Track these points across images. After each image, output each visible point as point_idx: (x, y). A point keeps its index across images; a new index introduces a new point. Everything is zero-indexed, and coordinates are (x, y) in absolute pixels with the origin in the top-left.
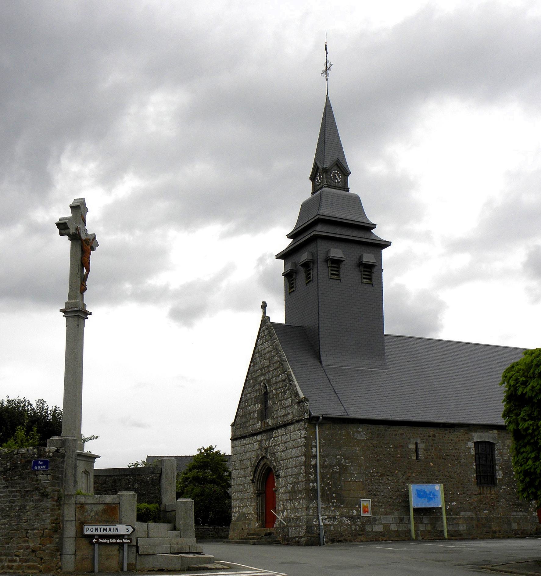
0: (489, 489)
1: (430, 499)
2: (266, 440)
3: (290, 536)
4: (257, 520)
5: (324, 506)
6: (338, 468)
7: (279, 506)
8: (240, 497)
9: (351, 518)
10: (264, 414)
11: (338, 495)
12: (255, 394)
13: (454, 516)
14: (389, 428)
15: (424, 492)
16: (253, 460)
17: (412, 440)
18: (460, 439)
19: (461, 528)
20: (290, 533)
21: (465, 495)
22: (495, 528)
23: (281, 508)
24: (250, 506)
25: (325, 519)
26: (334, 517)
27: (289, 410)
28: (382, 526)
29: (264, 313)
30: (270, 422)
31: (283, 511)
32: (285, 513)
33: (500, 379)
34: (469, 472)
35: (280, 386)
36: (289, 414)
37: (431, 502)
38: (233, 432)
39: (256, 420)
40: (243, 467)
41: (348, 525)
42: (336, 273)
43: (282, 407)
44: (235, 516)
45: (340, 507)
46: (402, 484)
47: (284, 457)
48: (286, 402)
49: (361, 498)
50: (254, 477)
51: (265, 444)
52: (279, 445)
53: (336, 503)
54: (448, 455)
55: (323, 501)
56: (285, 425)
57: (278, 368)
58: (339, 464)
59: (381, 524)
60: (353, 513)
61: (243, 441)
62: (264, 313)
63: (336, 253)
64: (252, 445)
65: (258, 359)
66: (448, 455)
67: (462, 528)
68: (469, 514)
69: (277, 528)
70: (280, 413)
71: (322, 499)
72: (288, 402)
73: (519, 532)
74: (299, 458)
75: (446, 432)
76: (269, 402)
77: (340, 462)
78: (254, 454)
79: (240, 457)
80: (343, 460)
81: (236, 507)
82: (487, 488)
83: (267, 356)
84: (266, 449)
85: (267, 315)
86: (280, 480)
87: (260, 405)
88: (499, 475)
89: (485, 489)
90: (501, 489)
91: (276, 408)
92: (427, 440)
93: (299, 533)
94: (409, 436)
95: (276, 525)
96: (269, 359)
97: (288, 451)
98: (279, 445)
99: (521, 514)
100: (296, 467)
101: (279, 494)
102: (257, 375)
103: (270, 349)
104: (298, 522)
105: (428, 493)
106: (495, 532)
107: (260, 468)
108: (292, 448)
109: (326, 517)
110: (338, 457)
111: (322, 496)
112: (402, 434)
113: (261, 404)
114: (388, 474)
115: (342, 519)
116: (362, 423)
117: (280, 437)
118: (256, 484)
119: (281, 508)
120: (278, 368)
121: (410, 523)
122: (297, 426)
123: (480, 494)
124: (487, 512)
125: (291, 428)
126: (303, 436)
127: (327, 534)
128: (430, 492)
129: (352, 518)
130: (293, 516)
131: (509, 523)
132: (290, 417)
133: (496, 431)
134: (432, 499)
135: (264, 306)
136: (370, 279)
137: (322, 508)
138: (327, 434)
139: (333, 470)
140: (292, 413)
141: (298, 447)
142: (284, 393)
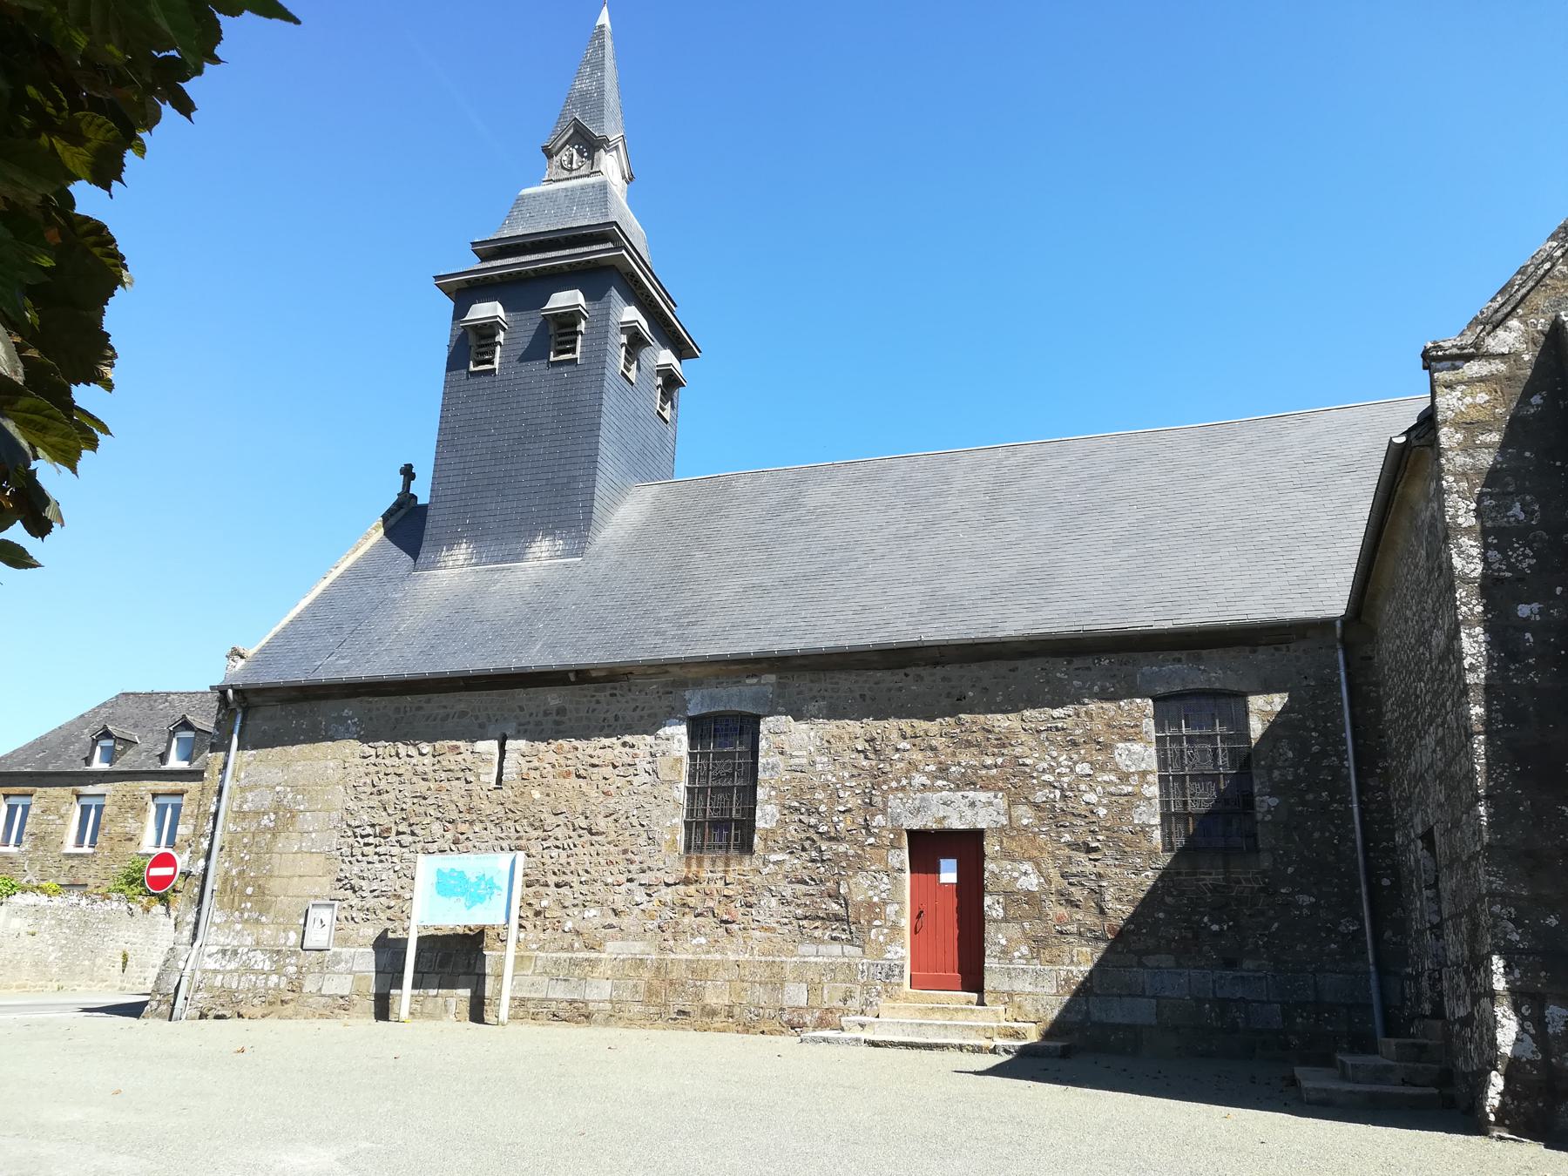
0: (720, 867)
1: (475, 899)
5: (218, 920)
6: (273, 817)
14: (429, 701)
17: (491, 728)
18: (646, 712)
22: (715, 997)
26: (235, 953)
29: (407, 486)
34: (656, 812)
37: (478, 908)
42: (93, 812)
45: (257, 921)
54: (593, 766)
60: (287, 938)
63: (565, 299)
66: (593, 766)
67: (599, 992)
68: (638, 948)
73: (808, 1018)
75: (601, 696)
82: (714, 862)
88: (766, 816)
89: (707, 864)
90: (765, 863)
92: (538, 724)
99: (836, 949)
105: (473, 880)
106: (713, 1013)
112: (463, 714)
114: (403, 827)
123: (687, 881)
124: (703, 940)
127: (198, 996)
128: (481, 878)
131: (776, 983)
133: (772, 678)
134: (481, 899)
138: (264, 732)
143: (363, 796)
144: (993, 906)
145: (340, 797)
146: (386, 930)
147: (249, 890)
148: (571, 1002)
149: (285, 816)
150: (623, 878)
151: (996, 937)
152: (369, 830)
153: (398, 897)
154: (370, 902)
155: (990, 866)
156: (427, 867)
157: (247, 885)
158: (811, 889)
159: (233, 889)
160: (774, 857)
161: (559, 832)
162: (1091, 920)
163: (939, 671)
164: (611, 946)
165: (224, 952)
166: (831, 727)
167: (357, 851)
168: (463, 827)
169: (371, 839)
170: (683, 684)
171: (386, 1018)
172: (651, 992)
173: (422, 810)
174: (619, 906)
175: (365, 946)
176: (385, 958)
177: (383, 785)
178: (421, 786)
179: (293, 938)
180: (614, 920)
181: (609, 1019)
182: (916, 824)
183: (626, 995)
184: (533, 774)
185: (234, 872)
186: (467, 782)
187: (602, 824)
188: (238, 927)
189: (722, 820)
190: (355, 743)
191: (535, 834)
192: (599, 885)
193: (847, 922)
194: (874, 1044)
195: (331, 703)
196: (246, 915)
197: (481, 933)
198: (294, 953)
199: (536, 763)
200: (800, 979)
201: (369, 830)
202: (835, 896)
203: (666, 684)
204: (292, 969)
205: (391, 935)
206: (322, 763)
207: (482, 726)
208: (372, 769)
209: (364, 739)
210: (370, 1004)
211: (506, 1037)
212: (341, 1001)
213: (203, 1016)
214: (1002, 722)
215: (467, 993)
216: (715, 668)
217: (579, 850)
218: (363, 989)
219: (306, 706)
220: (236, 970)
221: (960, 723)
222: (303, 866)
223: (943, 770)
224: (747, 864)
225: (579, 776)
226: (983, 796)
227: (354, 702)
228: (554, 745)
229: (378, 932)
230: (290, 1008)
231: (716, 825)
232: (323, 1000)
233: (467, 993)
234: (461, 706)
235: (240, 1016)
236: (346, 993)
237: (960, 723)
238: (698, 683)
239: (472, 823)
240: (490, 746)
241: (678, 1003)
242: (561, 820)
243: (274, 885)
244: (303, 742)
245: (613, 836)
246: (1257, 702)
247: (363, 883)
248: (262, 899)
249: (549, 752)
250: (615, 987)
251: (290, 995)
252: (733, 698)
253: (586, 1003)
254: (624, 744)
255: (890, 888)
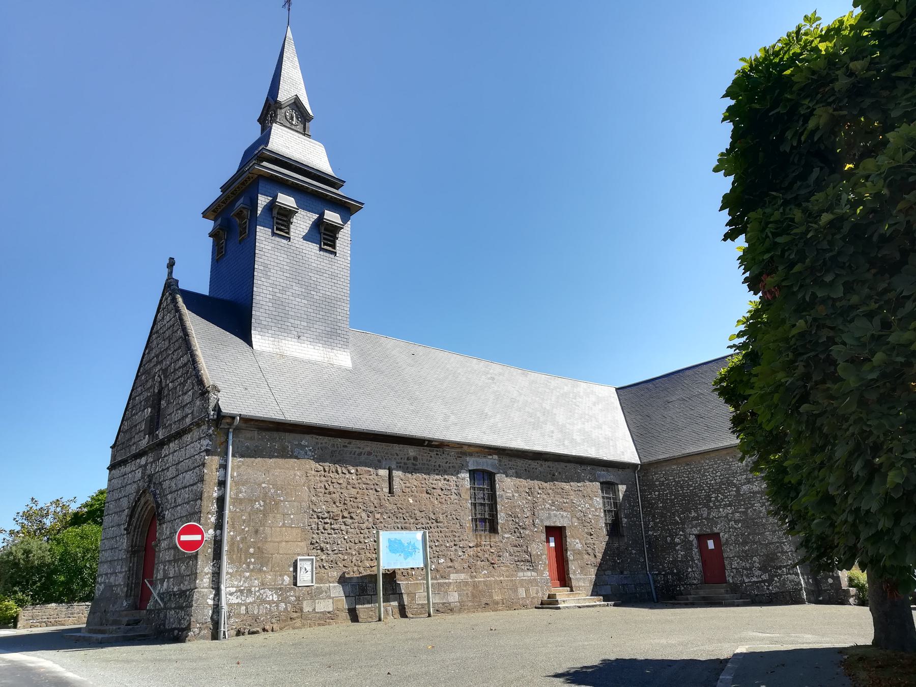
1: (408, 554)
2: (152, 463)
3: (167, 627)
4: (127, 596)
5: (230, 571)
6: (262, 503)
7: (158, 571)
8: (109, 559)
9: (280, 590)
10: (154, 423)
11: (260, 550)
12: (146, 394)
13: (441, 581)
14: (350, 443)
15: (400, 542)
16: (132, 497)
17: (384, 463)
19: (451, 599)
20: (167, 622)
21: (457, 548)
23: (160, 575)
24: (121, 572)
25: (231, 594)
26: (249, 591)
27: (188, 411)
28: (331, 601)
29: (170, 273)
30: (161, 434)
31: (162, 581)
32: (165, 584)
33: (728, 81)
34: (462, 513)
35: (180, 374)
36: (186, 416)
37: (409, 559)
38: (114, 457)
39: (142, 434)
40: (118, 510)
41: (273, 601)
43: (178, 406)
44: (99, 589)
45: (260, 570)
46: (366, 531)
47: (174, 488)
48: (186, 397)
49: (299, 555)
50: (129, 525)
51: (150, 470)
52: (168, 468)
53: (253, 564)
55: (231, 561)
56: (179, 435)
57: (180, 348)
58: (265, 497)
59: (330, 597)
61: (123, 469)
62: (170, 273)
63: (286, 200)
64: (134, 472)
65: (155, 342)
67: (454, 597)
68: (462, 576)
69: (150, 611)
70: (174, 417)
71: (229, 558)
72: (187, 398)
74: (195, 487)
75: (433, 454)
76: (163, 402)
77: (266, 494)
78: (135, 486)
79: (116, 495)
80: (272, 491)
81: (101, 575)
83: (167, 334)
84: (151, 477)
85: (174, 276)
86: (164, 526)
87: (150, 410)
90: (503, 538)
91: (170, 410)
93: (180, 623)
94: (379, 458)
95: (150, 605)
96: (169, 339)
97: (181, 476)
98: (168, 468)
99: (529, 574)
100: (188, 503)
101: (160, 551)
102: (152, 365)
103: (171, 322)
104: (181, 601)
106: (497, 603)
107: (139, 509)
108: (186, 472)
109: (234, 590)
110: (263, 485)
111: (230, 552)
112: (369, 454)
113: (153, 407)
115: (262, 591)
116: (308, 433)
117: (171, 456)
118: (132, 533)
119: (160, 575)
120: (180, 348)
121: (376, 594)
122: (196, 433)
123: (477, 546)
125: (187, 438)
126: (203, 448)
127: (232, 620)
128: (409, 544)
129: (280, 589)
130: (175, 589)
132: (188, 420)
133: (496, 457)
135: (171, 264)
136: (334, 247)
137: (227, 573)
138: (247, 447)
139: (253, 507)
140: (192, 413)
141: (194, 468)
142: (183, 384)
143: (320, 495)
144: (570, 555)
145: (305, 493)
146: (344, 573)
147: (252, 550)
148: (443, 604)
149: (271, 505)
150: (452, 544)
151: (573, 566)
152: (326, 515)
153: (349, 554)
154: (333, 557)
155: (568, 540)
156: (385, 537)
157: (249, 547)
158: (519, 549)
159: (240, 550)
160: (506, 536)
161: (424, 521)
162: (593, 559)
163: (548, 463)
164: (453, 576)
165: (241, 591)
166: (518, 481)
167: (321, 527)
168: (378, 516)
169: (327, 520)
170: (465, 454)
171: (357, 621)
172: (474, 596)
173: (355, 505)
174: (453, 557)
175: (333, 582)
176: (348, 588)
177: (331, 489)
178: (353, 492)
179: (287, 579)
180: (450, 564)
181: (460, 610)
182: (548, 523)
183: (465, 599)
184: (407, 490)
185: (238, 538)
186: (376, 491)
187: (441, 517)
188: (247, 574)
189: (488, 521)
190: (312, 462)
191: (412, 521)
192: (443, 548)
193: (531, 563)
194: (579, 607)
195: (292, 435)
196: (251, 567)
197: (394, 572)
198: (291, 589)
199: (408, 485)
200: (522, 586)
201: (326, 515)
202: (526, 552)
203: (458, 453)
204: (293, 599)
205: (347, 576)
206: (292, 472)
207: (379, 461)
208: (323, 479)
209: (318, 460)
210: (345, 615)
211: (415, 625)
212: (329, 615)
213: (239, 633)
214: (566, 486)
215: (395, 604)
216: (477, 449)
217: (432, 530)
218: (340, 607)
219: (275, 435)
220: (254, 602)
221: (554, 485)
222: (286, 535)
223: (553, 504)
224: (496, 539)
225: (427, 493)
226: (565, 514)
227: (308, 437)
228: (415, 476)
229: (340, 574)
230: (298, 623)
231: (483, 520)
232: (318, 615)
233: (395, 604)
234: (368, 449)
235: (264, 630)
236: (331, 609)
237: (554, 485)
238: (471, 455)
239: (382, 514)
240: (384, 473)
241: (484, 600)
242: (423, 514)
243: (269, 547)
244: (277, 457)
245: (446, 524)
246: (620, 487)
247: (328, 546)
248: (262, 557)
249: (415, 479)
250: (459, 595)
251: (295, 615)
252: (488, 463)
253: (449, 603)
254: (445, 479)
255: (543, 549)
